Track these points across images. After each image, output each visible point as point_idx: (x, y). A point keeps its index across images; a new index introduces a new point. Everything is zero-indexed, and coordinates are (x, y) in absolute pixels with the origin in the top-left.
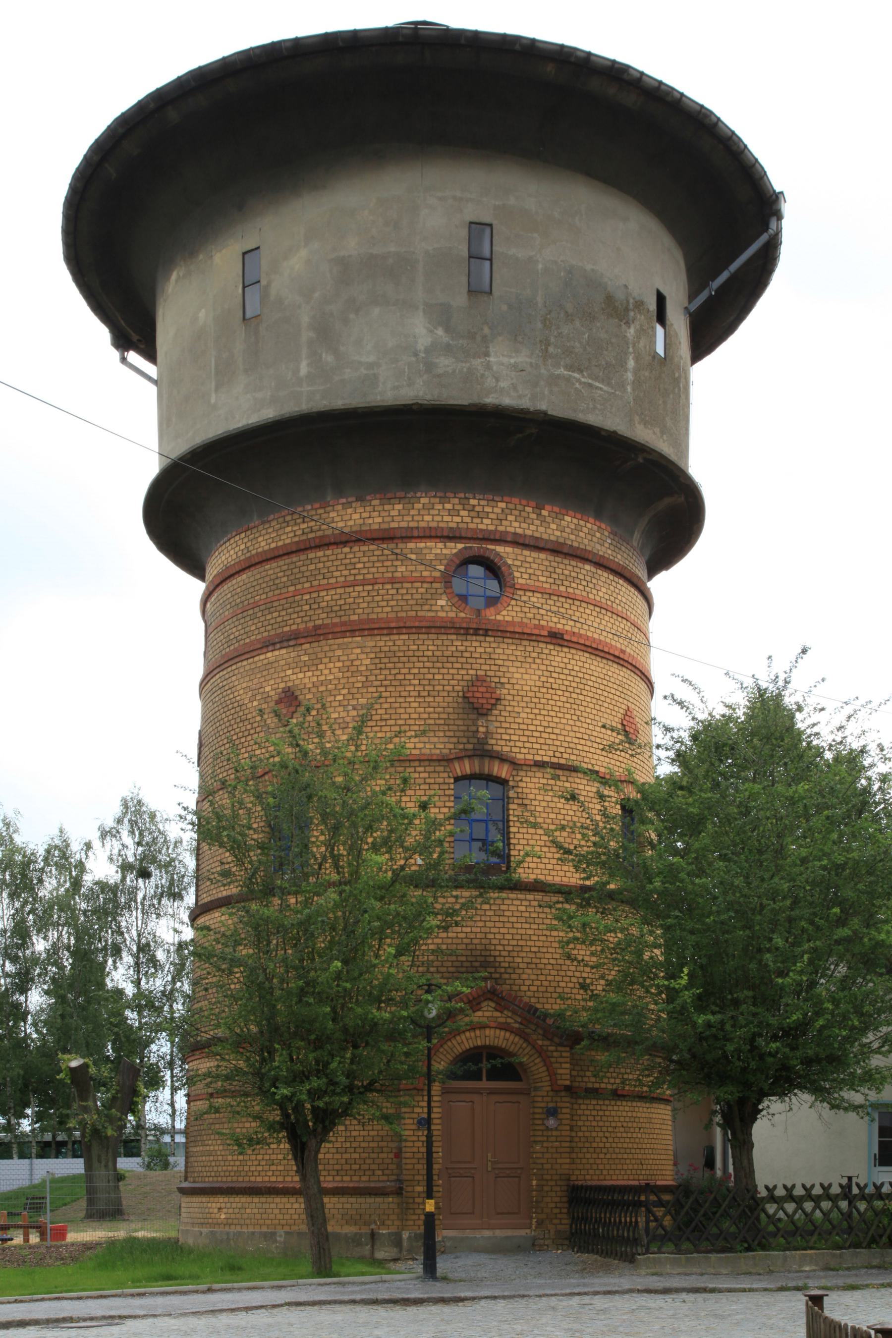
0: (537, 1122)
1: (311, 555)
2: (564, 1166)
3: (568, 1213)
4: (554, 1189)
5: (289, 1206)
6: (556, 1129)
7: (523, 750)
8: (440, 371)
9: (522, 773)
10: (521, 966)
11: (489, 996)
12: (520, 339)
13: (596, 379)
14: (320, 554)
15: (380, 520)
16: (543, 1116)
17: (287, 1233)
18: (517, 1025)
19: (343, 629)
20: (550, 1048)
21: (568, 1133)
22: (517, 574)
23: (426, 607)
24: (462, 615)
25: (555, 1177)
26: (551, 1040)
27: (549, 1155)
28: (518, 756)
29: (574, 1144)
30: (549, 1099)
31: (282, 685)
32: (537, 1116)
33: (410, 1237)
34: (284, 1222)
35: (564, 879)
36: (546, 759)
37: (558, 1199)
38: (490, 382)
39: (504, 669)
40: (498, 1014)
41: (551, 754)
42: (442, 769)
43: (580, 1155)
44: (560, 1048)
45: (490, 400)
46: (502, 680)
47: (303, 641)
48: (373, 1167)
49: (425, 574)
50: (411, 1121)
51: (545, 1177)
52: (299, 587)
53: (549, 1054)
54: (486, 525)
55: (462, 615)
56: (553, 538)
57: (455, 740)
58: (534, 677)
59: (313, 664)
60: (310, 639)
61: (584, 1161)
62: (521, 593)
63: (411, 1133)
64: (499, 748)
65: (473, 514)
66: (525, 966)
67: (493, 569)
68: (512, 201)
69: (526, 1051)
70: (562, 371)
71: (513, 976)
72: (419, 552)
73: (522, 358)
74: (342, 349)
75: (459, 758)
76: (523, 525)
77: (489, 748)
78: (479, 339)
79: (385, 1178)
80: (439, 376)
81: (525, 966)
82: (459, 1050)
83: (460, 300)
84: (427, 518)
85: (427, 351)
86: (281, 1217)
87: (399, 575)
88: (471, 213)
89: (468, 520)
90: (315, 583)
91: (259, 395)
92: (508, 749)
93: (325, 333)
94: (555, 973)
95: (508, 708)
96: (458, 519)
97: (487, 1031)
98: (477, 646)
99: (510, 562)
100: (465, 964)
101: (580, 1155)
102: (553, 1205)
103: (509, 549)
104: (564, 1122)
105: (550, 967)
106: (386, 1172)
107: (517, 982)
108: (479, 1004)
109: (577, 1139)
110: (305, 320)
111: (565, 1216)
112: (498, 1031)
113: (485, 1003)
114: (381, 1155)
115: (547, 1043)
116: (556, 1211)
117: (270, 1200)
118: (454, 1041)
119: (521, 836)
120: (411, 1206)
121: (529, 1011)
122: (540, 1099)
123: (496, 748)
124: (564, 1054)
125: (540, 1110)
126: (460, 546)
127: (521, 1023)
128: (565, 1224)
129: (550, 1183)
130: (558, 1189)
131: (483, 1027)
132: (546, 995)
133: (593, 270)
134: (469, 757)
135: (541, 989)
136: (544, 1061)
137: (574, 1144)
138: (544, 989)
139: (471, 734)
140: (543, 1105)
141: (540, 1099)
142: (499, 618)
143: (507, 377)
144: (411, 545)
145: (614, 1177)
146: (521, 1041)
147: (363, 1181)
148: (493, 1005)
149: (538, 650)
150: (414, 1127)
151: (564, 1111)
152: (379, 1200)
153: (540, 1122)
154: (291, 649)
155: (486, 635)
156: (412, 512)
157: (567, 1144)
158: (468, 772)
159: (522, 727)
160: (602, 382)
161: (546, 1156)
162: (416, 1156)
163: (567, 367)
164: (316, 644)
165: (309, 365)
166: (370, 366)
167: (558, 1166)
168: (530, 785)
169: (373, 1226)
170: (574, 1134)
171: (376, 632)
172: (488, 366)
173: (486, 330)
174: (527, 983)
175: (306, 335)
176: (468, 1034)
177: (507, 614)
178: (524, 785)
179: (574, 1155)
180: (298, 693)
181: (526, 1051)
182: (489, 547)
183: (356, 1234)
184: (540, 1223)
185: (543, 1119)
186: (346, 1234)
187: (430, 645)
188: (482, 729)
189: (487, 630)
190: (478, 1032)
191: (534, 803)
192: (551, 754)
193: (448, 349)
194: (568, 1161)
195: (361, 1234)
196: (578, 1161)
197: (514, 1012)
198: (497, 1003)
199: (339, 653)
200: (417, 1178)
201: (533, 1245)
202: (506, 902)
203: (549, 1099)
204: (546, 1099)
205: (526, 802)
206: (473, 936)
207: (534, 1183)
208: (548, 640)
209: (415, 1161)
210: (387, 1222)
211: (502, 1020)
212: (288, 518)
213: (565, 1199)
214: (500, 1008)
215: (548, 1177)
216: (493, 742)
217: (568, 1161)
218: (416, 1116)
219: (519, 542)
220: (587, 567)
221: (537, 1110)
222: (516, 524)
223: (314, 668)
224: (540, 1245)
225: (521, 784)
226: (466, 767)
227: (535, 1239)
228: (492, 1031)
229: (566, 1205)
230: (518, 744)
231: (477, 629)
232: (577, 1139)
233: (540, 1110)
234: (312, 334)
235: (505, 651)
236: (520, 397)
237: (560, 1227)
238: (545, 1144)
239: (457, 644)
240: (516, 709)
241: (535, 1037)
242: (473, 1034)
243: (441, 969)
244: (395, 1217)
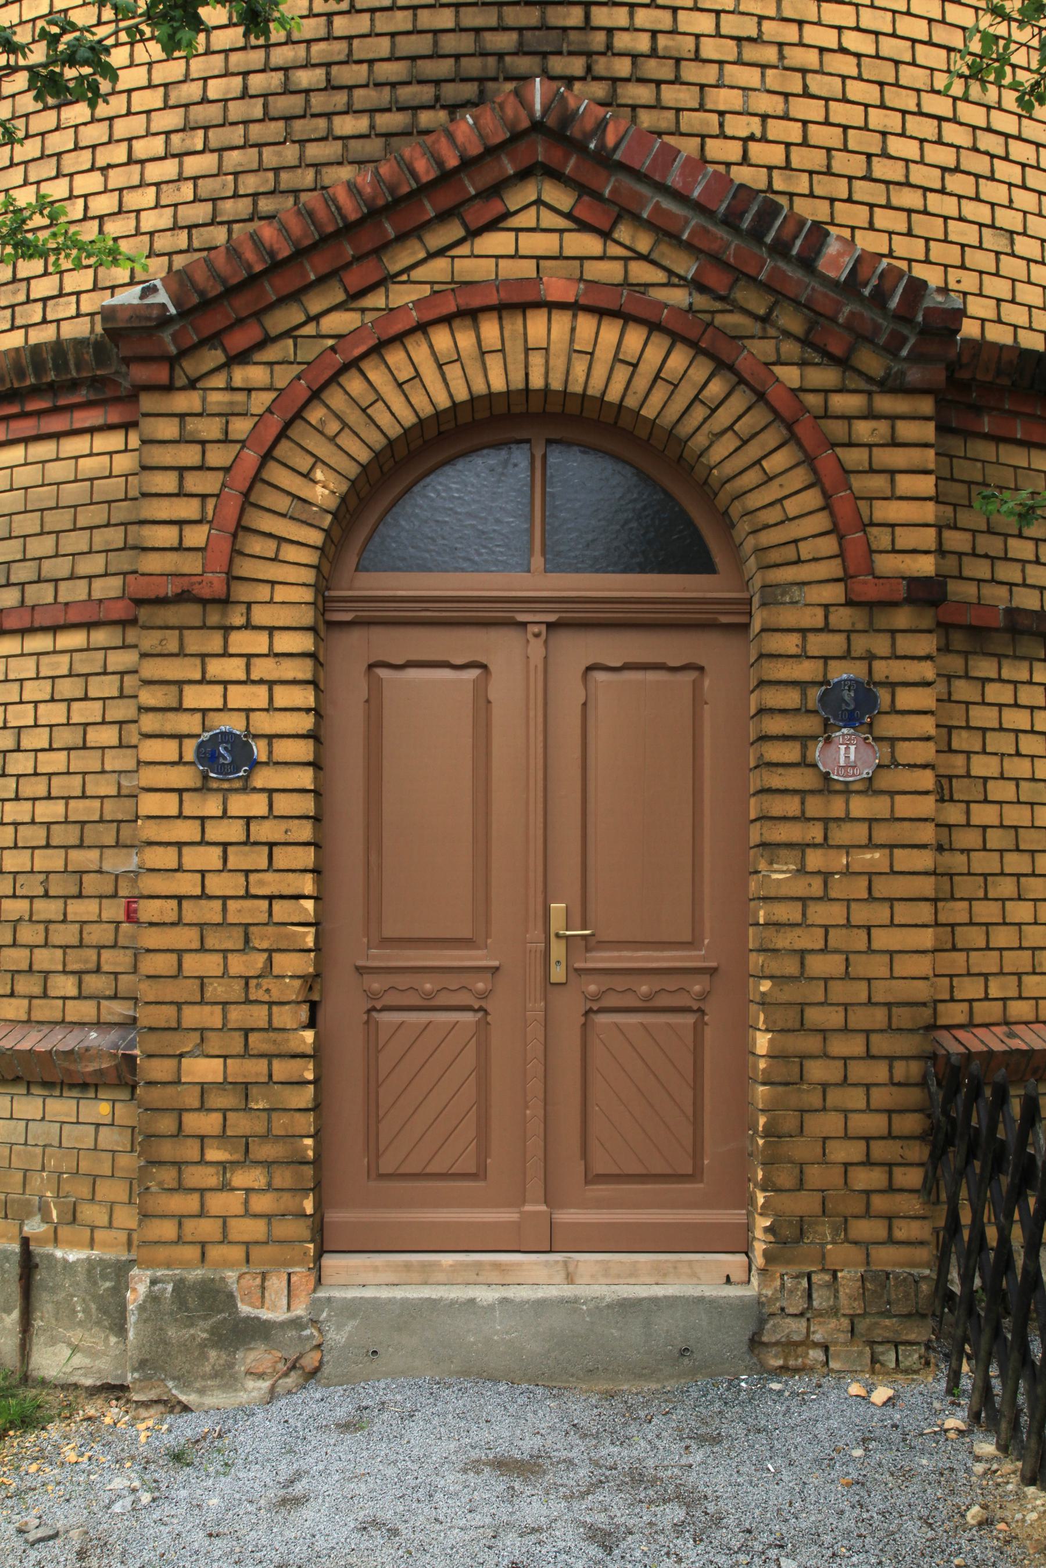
0: (775, 752)
2: (906, 966)
3: (928, 1190)
4: (859, 1071)
6: (870, 788)
10: (710, 49)
11: (541, 151)
16: (808, 725)
18: (678, 297)
20: (840, 402)
21: (927, 806)
25: (860, 1018)
26: (843, 363)
27: (835, 913)
29: (957, 862)
30: (835, 643)
32: (775, 725)
33: (153, 1299)
37: (876, 1124)
40: (589, 244)
43: (987, 912)
44: (885, 403)
48: (46, 959)
50: (168, 750)
51: (814, 1016)
53: (837, 429)
61: (1002, 937)
63: (169, 804)
66: (728, 50)
69: (723, 417)
71: (671, 95)
79: (86, 1010)
81: (728, 50)
94: (870, 93)
97: (537, 325)
100: (449, 43)
101: (987, 912)
102: (855, 1151)
104: (907, 752)
105: (846, 65)
106: (94, 983)
107: (690, 121)
108: (496, 190)
109: (969, 839)
111: (913, 1204)
112: (586, 324)
113: (528, 192)
114: (78, 909)
115: (824, 376)
116: (865, 1179)
118: (377, 375)
120: (167, 1150)
121: (730, 221)
122: (790, 643)
124: (907, 431)
125: (790, 698)
127: (698, 285)
128: (909, 1251)
129: (839, 1046)
130: (879, 1072)
131: (517, 302)
132: (824, 186)
135: (800, 158)
136: (809, 461)
137: (957, 862)
138: (816, 159)
140: (806, 671)
141: (790, 643)
146: (700, 372)
148: (561, 197)
151: (906, 698)
152: (61, 1107)
153: (790, 753)
157: (924, 860)
161: (820, 913)
162: (192, 912)
167: (878, 967)
169: (34, 1227)
170: (954, 814)
174: (739, 127)
176: (441, 338)
179: (957, 912)
181: (723, 417)
184: (789, 1237)
185: (804, 740)
190: (490, 330)
194: (926, 938)
196: (975, 937)
197: (665, 233)
198: (581, 189)
200: (192, 1016)
201: (755, 1343)
203: (835, 643)
204: (817, 644)
207: (762, 1042)
209: (187, 938)
210: (90, 1213)
211: (610, 272)
213: (910, 1124)
214: (600, 215)
217: (926, 938)
218: (189, 724)
221: (776, 698)
224: (789, 1346)
227: (760, 1315)
228: (561, 322)
229: (918, 1152)
232: (969, 839)
233: (790, 698)
237: (885, 1257)
238: (815, 860)
241: (763, 349)
242: (466, 340)
243: (345, 75)
244: (117, 1191)
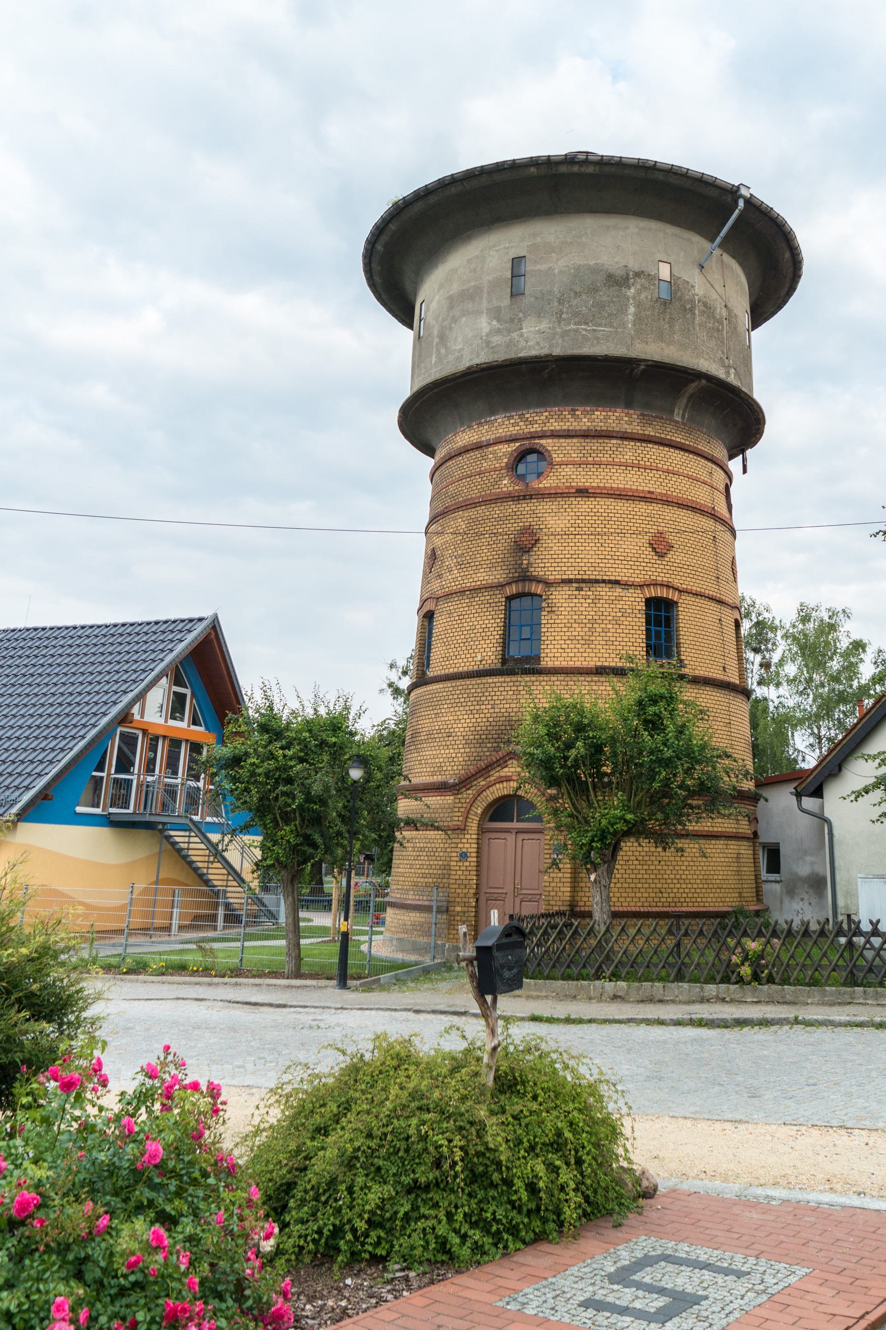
7: (554, 573)
8: (494, 345)
9: (552, 589)
12: (542, 315)
13: (600, 325)
15: (476, 437)
22: (554, 456)
23: (496, 487)
24: (517, 488)
25: (558, 903)
27: (554, 884)
28: (550, 577)
35: (570, 663)
36: (571, 577)
38: (523, 343)
39: (543, 519)
41: (577, 573)
42: (498, 592)
45: (522, 354)
46: (541, 527)
49: (497, 465)
54: (536, 428)
55: (517, 488)
56: (584, 428)
57: (507, 571)
58: (564, 522)
62: (558, 467)
64: (536, 573)
65: (527, 423)
67: (540, 453)
68: (539, 240)
70: (572, 326)
72: (494, 453)
73: (544, 325)
75: (509, 584)
76: (561, 424)
77: (529, 574)
78: (516, 321)
80: (493, 348)
82: (491, 798)
83: (506, 301)
84: (500, 431)
85: (487, 335)
87: (483, 469)
88: (514, 253)
89: (524, 427)
92: (543, 573)
95: (544, 545)
96: (518, 428)
98: (525, 507)
99: (549, 448)
103: (550, 441)
108: (506, 761)
110: (436, 332)
113: (511, 762)
119: (549, 634)
123: (534, 574)
126: (517, 444)
133: (596, 264)
134: (516, 582)
139: (517, 566)
142: (541, 486)
143: (535, 338)
144: (491, 449)
145: (707, 904)
149: (568, 503)
150: (457, 859)
155: (531, 499)
159: (554, 556)
160: (605, 326)
163: (575, 324)
167: (561, 894)
168: (558, 597)
172: (522, 335)
173: (521, 315)
175: (436, 340)
177: (546, 483)
178: (553, 597)
182: (537, 441)
187: (496, 511)
188: (525, 562)
189: (531, 495)
190: (505, 784)
191: (560, 609)
192: (577, 573)
193: (498, 331)
200: (457, 900)
202: (535, 683)
205: (554, 609)
206: (510, 710)
208: (577, 495)
215: (554, 903)
216: (533, 569)
218: (458, 850)
219: (554, 435)
220: (614, 441)
222: (556, 424)
225: (551, 597)
226: (513, 589)
230: (550, 569)
231: (524, 496)
235: (544, 507)
236: (542, 348)
239: (512, 507)
240: (550, 545)
242: (501, 786)
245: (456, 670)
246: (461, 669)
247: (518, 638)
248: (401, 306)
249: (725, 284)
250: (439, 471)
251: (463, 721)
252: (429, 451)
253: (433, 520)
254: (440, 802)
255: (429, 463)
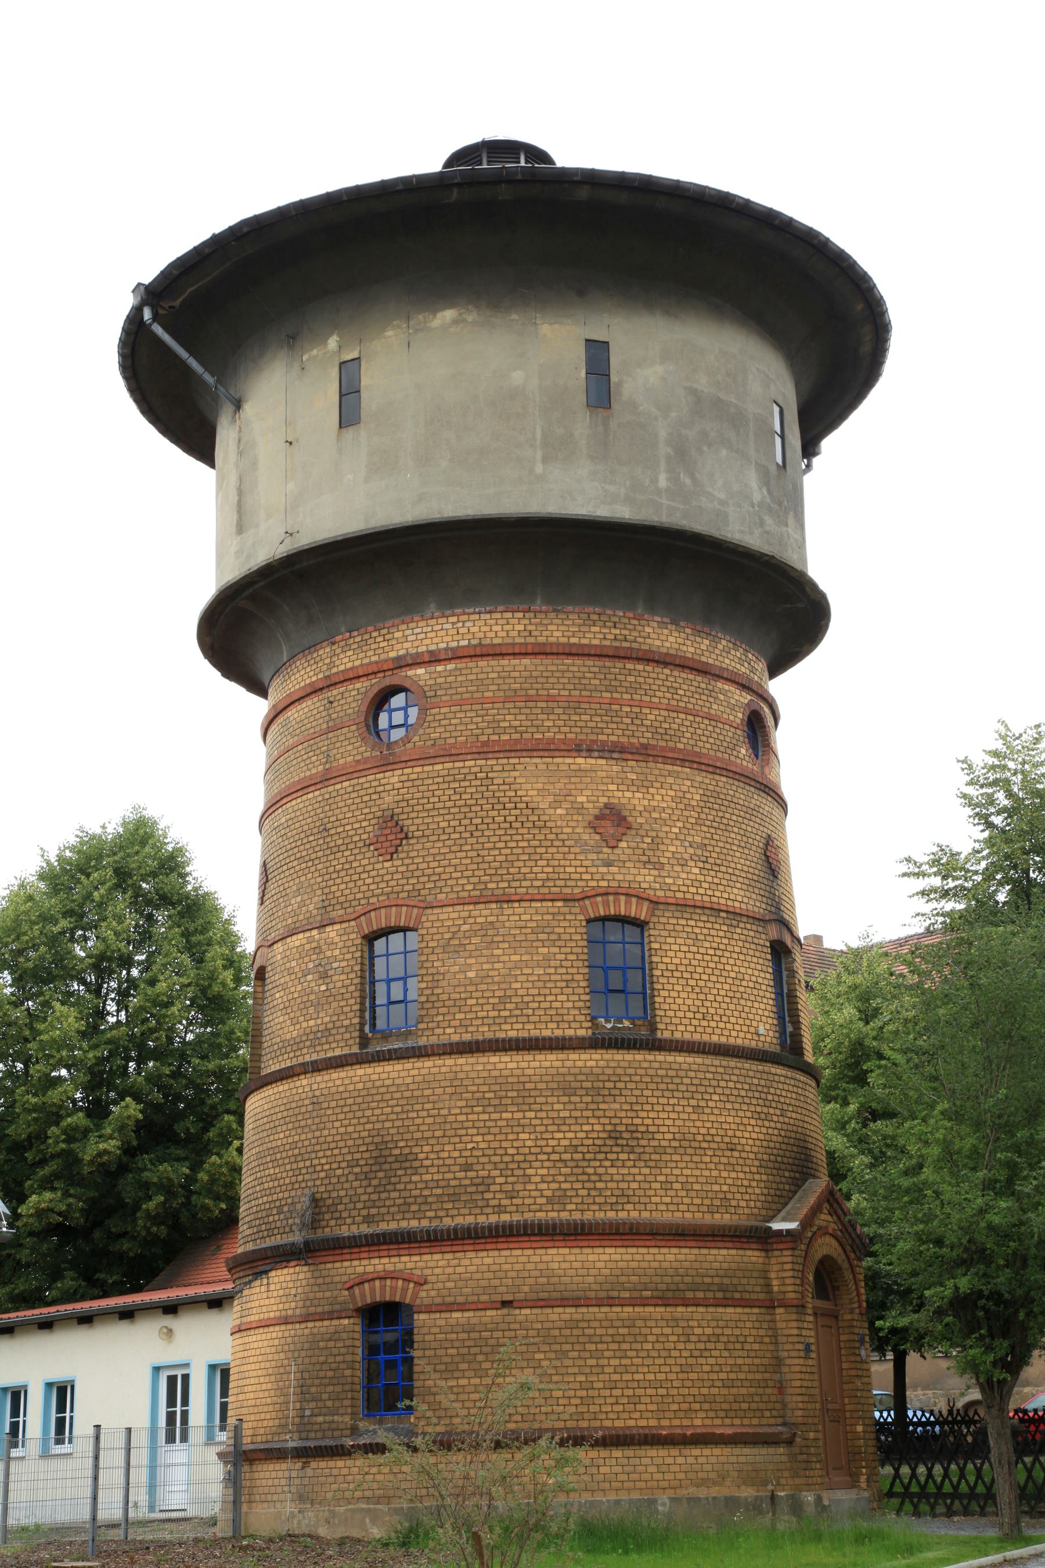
1: (630, 666)
5: (670, 1460)
14: (640, 667)
15: (692, 650)
17: (673, 1500)
19: (675, 755)
31: (605, 800)
34: (665, 1484)
47: (630, 757)
52: (615, 695)
59: (643, 785)
60: (637, 757)
74: (697, 476)
86: (660, 1476)
90: (637, 697)
91: (611, 488)
93: (682, 455)
110: (663, 434)
117: (641, 1452)
147: (699, 1423)
154: (613, 762)
156: (717, 651)
158: (602, 913)
164: (643, 764)
165: (668, 479)
166: (722, 503)
171: (703, 767)
175: (664, 450)
180: (626, 813)
183: (756, 1498)
186: (746, 1498)
195: (761, 1498)
199: (670, 780)
212: (595, 617)
223: (644, 790)
234: (669, 450)
245: (723, 1040)
246: (732, 1041)
247: (385, 1002)
248: (194, 435)
249: (761, 376)
250: (280, 720)
251: (345, 1151)
252: (259, 688)
253: (272, 807)
254: (738, 1259)
255: (259, 707)
